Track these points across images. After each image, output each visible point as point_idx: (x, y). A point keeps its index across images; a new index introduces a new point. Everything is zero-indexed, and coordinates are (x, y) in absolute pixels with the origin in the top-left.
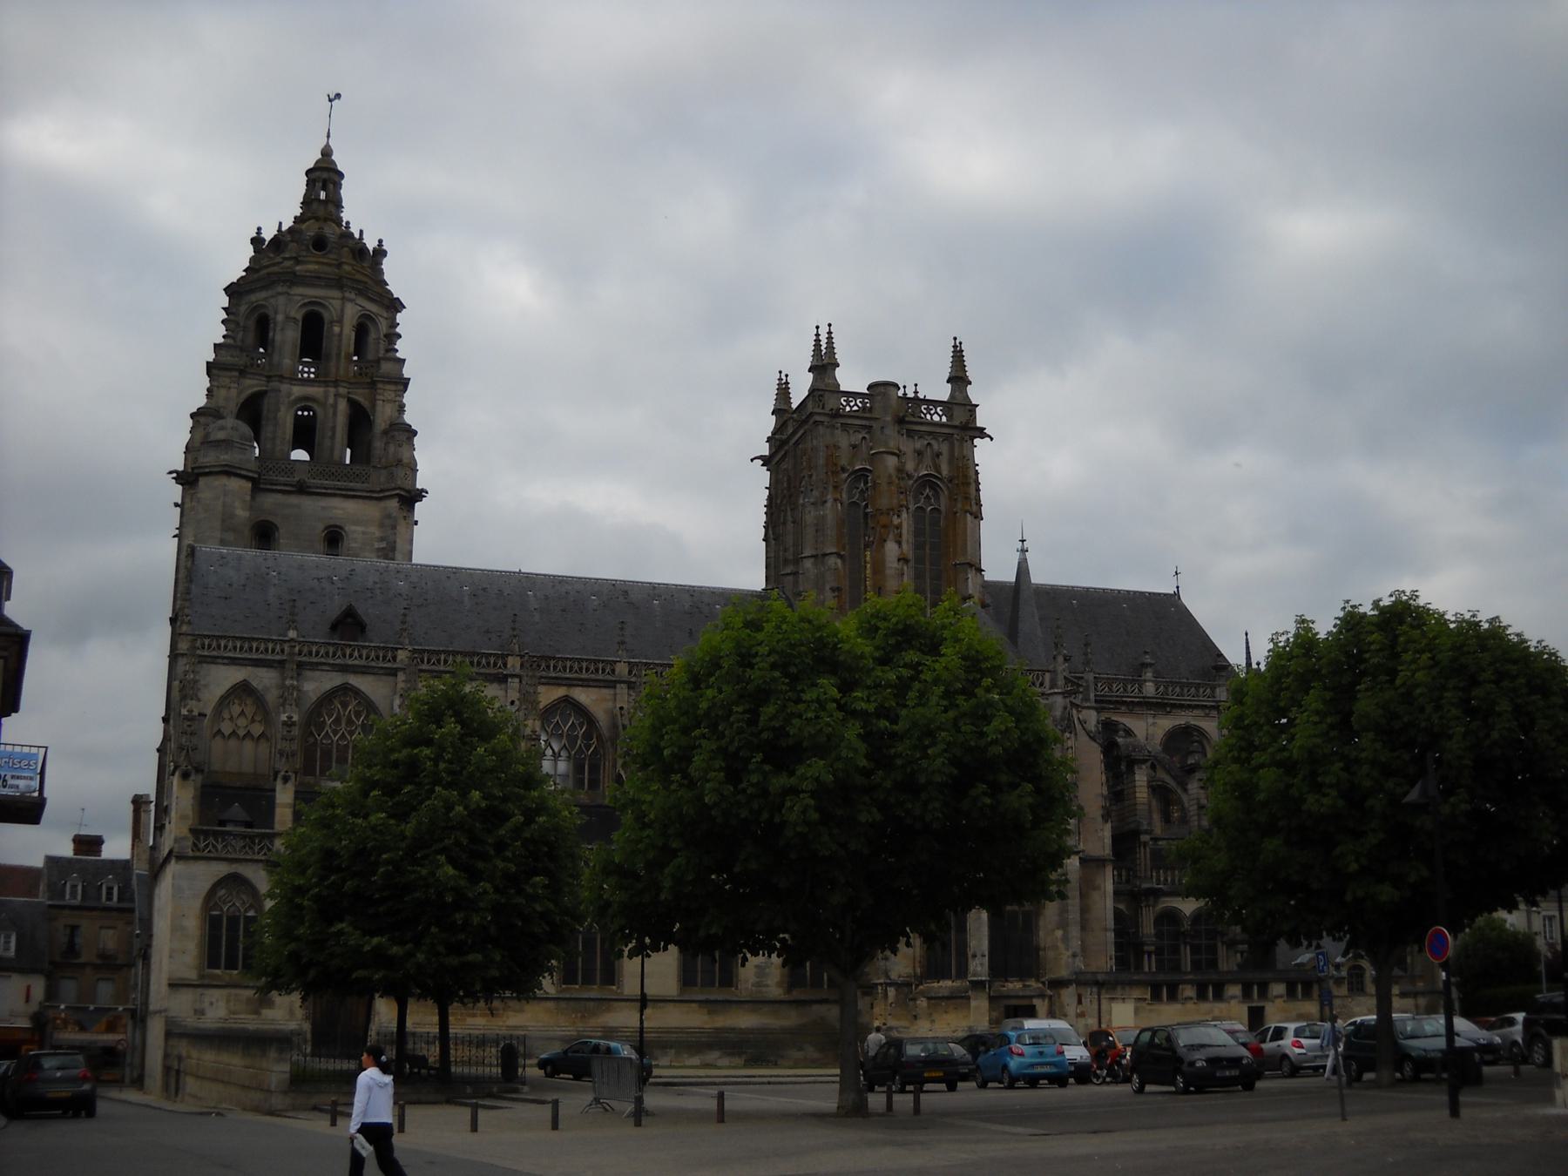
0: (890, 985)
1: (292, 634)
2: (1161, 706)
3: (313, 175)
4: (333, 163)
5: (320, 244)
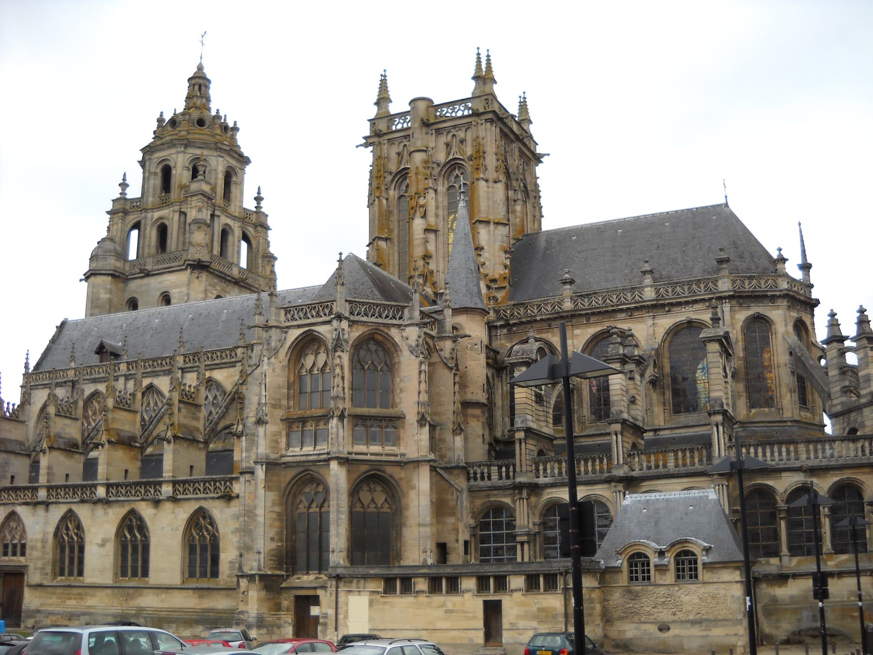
0: (242, 576)
1: (73, 365)
2: (658, 307)
3: (193, 82)
4: (204, 74)
5: (201, 122)
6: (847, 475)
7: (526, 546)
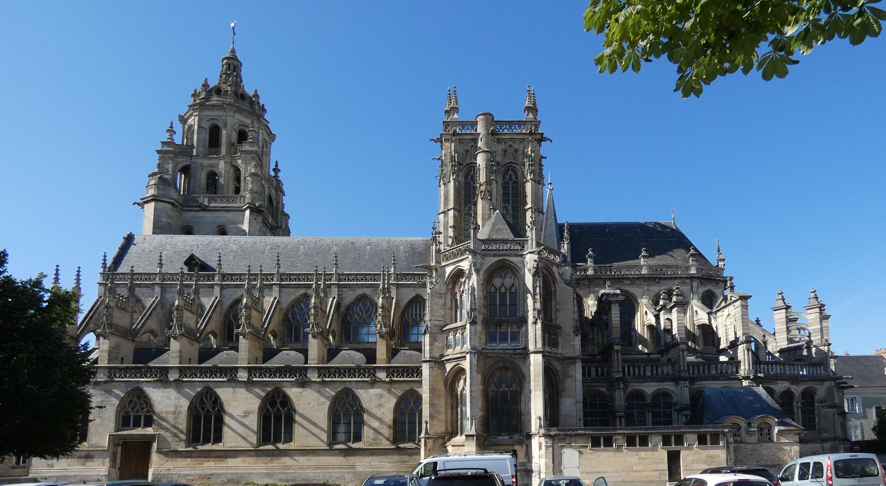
0: (428, 438)
6: (810, 384)
7: (623, 419)
